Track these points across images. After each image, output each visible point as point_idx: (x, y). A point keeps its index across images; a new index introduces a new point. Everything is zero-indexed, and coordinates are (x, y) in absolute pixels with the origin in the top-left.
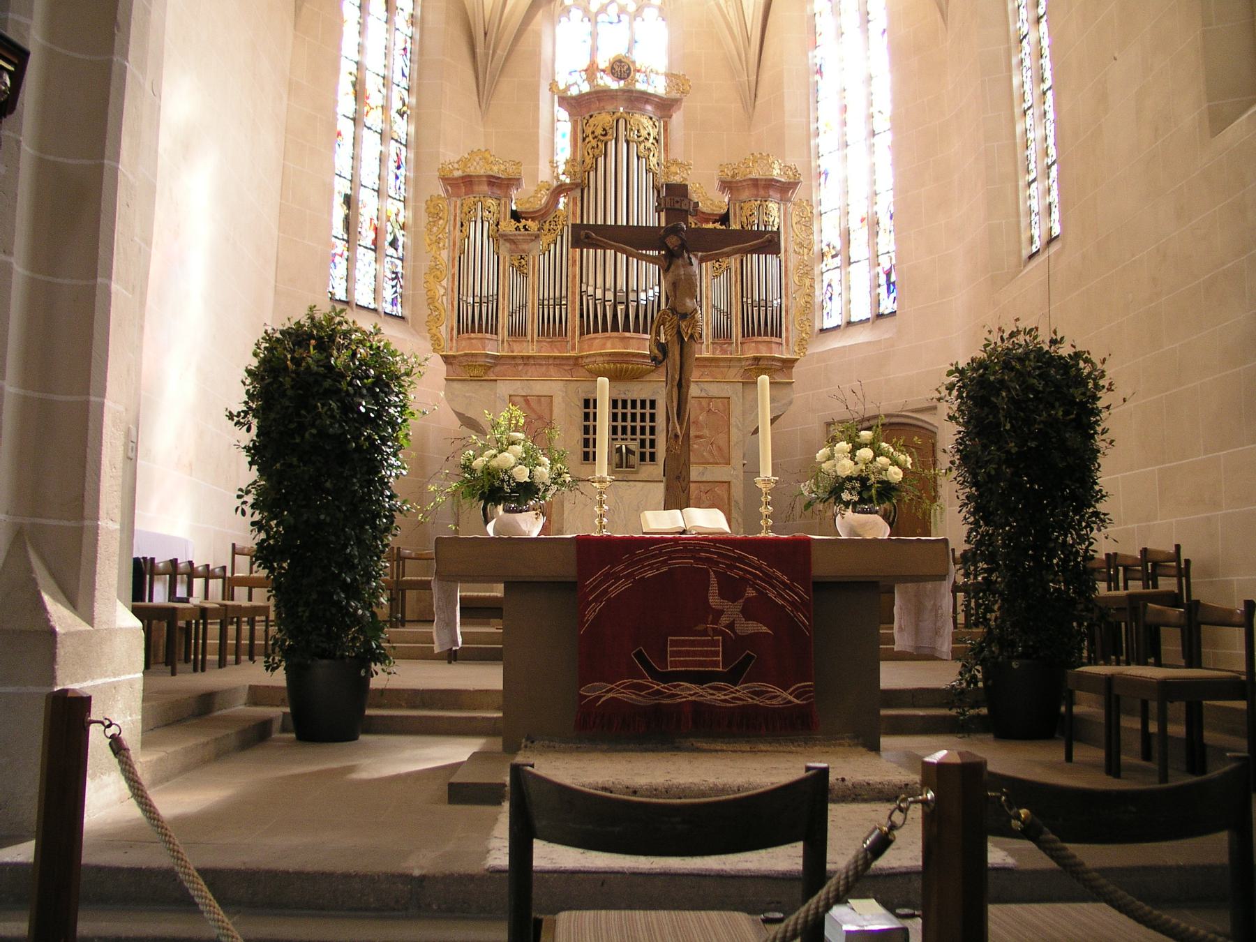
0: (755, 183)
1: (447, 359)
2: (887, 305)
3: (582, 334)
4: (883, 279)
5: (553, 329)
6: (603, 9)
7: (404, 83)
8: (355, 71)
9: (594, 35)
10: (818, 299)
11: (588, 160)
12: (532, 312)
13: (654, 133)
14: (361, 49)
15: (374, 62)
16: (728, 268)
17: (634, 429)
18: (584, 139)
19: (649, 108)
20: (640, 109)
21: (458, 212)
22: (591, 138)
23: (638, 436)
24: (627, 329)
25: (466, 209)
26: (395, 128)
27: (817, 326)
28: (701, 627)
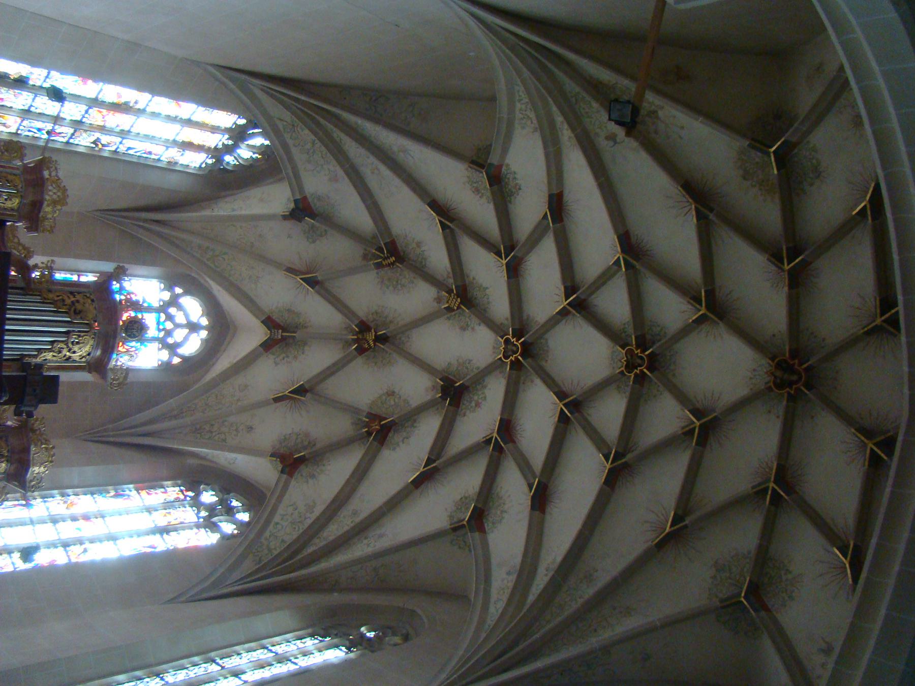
0: (27, 450)
7: (122, 149)
8: (137, 107)
13: (75, 356)
14: (155, 115)
15: (142, 125)
18: (72, 293)
19: (99, 353)
20: (98, 345)
21: (9, 170)
22: (73, 299)
25: (10, 177)
26: (84, 135)
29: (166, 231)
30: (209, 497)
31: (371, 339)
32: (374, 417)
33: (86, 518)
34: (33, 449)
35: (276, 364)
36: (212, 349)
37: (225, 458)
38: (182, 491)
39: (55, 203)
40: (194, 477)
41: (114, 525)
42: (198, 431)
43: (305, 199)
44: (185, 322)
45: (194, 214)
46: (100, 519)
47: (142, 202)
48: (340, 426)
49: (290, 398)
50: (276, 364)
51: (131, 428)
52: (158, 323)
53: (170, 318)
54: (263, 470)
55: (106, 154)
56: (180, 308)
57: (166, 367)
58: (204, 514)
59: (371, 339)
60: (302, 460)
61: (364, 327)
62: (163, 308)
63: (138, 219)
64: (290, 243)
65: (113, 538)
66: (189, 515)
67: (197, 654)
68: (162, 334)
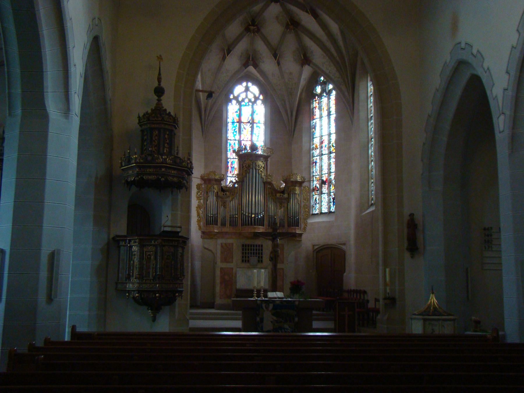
1: (203, 233)
2: (333, 209)
3: (242, 225)
4: (332, 200)
5: (233, 223)
9: (240, 110)
11: (244, 174)
12: (228, 219)
13: (263, 166)
16: (284, 206)
17: (256, 253)
19: (262, 159)
23: (258, 255)
24: (255, 225)
27: (311, 213)
29: (209, 108)
30: (318, 89)
32: (287, 27)
34: (292, 180)
35: (263, 62)
36: (256, 82)
37: (303, 83)
38: (315, 101)
39: (215, 175)
40: (311, 96)
41: (325, 132)
44: (245, 93)
45: (201, 97)
46: (323, 137)
48: (291, 38)
49: (278, 60)
50: (263, 62)
51: (288, 119)
52: (246, 105)
53: (243, 100)
54: (307, 71)
56: (239, 96)
57: (264, 102)
60: (305, 55)
62: (239, 103)
63: (205, 120)
65: (330, 135)
66: (325, 100)
67: (368, 123)
68: (250, 104)
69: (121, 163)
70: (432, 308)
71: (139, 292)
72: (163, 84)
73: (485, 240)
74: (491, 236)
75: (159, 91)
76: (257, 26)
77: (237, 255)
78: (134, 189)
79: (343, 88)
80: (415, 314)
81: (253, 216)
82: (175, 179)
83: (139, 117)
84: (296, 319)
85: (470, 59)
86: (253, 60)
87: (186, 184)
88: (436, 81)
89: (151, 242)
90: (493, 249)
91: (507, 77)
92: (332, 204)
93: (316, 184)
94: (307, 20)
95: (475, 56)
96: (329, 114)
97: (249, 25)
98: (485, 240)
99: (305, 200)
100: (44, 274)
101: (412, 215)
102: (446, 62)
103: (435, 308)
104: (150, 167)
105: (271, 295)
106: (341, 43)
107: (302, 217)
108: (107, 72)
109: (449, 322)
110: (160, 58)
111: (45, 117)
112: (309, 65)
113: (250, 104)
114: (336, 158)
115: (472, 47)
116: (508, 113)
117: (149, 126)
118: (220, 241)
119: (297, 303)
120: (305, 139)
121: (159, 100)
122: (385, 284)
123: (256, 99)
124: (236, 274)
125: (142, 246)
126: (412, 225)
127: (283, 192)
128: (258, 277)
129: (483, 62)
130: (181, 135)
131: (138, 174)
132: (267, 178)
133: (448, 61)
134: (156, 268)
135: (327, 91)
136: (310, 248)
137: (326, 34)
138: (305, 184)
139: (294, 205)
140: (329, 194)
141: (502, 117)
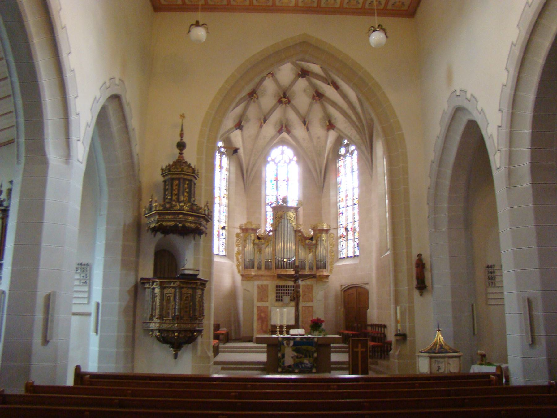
0: (319, 230)
1: (242, 275)
2: (357, 253)
4: (356, 246)
6: (279, 162)
7: (225, 188)
10: (339, 249)
24: (287, 268)
28: (237, 394)
30: (343, 151)
31: (284, 98)
32: (313, 98)
33: (347, 196)
39: (252, 225)
40: (337, 156)
42: (320, 155)
43: (235, 126)
47: (241, 178)
48: (317, 107)
54: (332, 135)
55: (227, 193)
57: (298, 162)
58: (348, 154)
59: (284, 98)
61: (280, 102)
64: (251, 128)
66: (348, 158)
69: (145, 211)
70: (438, 346)
71: (160, 331)
72: (185, 140)
73: (489, 277)
74: (494, 273)
75: (181, 146)
76: (287, 98)
77: (272, 296)
78: (159, 236)
79: (363, 148)
80: (421, 352)
81: (285, 260)
82: (193, 225)
83: (162, 169)
84: (315, 355)
85: (465, 104)
86: (286, 127)
87: (204, 229)
88: (437, 129)
89: (170, 284)
90: (497, 286)
91: (500, 114)
92: (356, 249)
93: (342, 231)
94: (329, 91)
95: (469, 101)
96: (353, 171)
97: (281, 98)
98: (489, 277)
99: (331, 245)
100: (39, 316)
101: (420, 255)
102: (444, 110)
103: (441, 346)
104: (169, 214)
105: (292, 332)
106: (359, 109)
107: (329, 261)
108: (134, 129)
109: (455, 359)
110: (183, 116)
111: (45, 162)
112: (333, 130)
113: (286, 165)
114: (360, 208)
115: (466, 92)
116: (503, 149)
117: (169, 176)
118: (257, 283)
119: (316, 340)
120: (332, 193)
121: (181, 154)
122: (397, 322)
123: (291, 160)
124: (271, 312)
125: (162, 288)
126: (420, 265)
127: (311, 239)
128: (283, 315)
129: (477, 104)
130: (203, 185)
131: (158, 221)
132: (297, 227)
133: (446, 110)
134: (175, 309)
135: (350, 151)
136: (339, 289)
137: (346, 102)
138: (331, 231)
139: (321, 251)
140: (354, 240)
141: (498, 154)
